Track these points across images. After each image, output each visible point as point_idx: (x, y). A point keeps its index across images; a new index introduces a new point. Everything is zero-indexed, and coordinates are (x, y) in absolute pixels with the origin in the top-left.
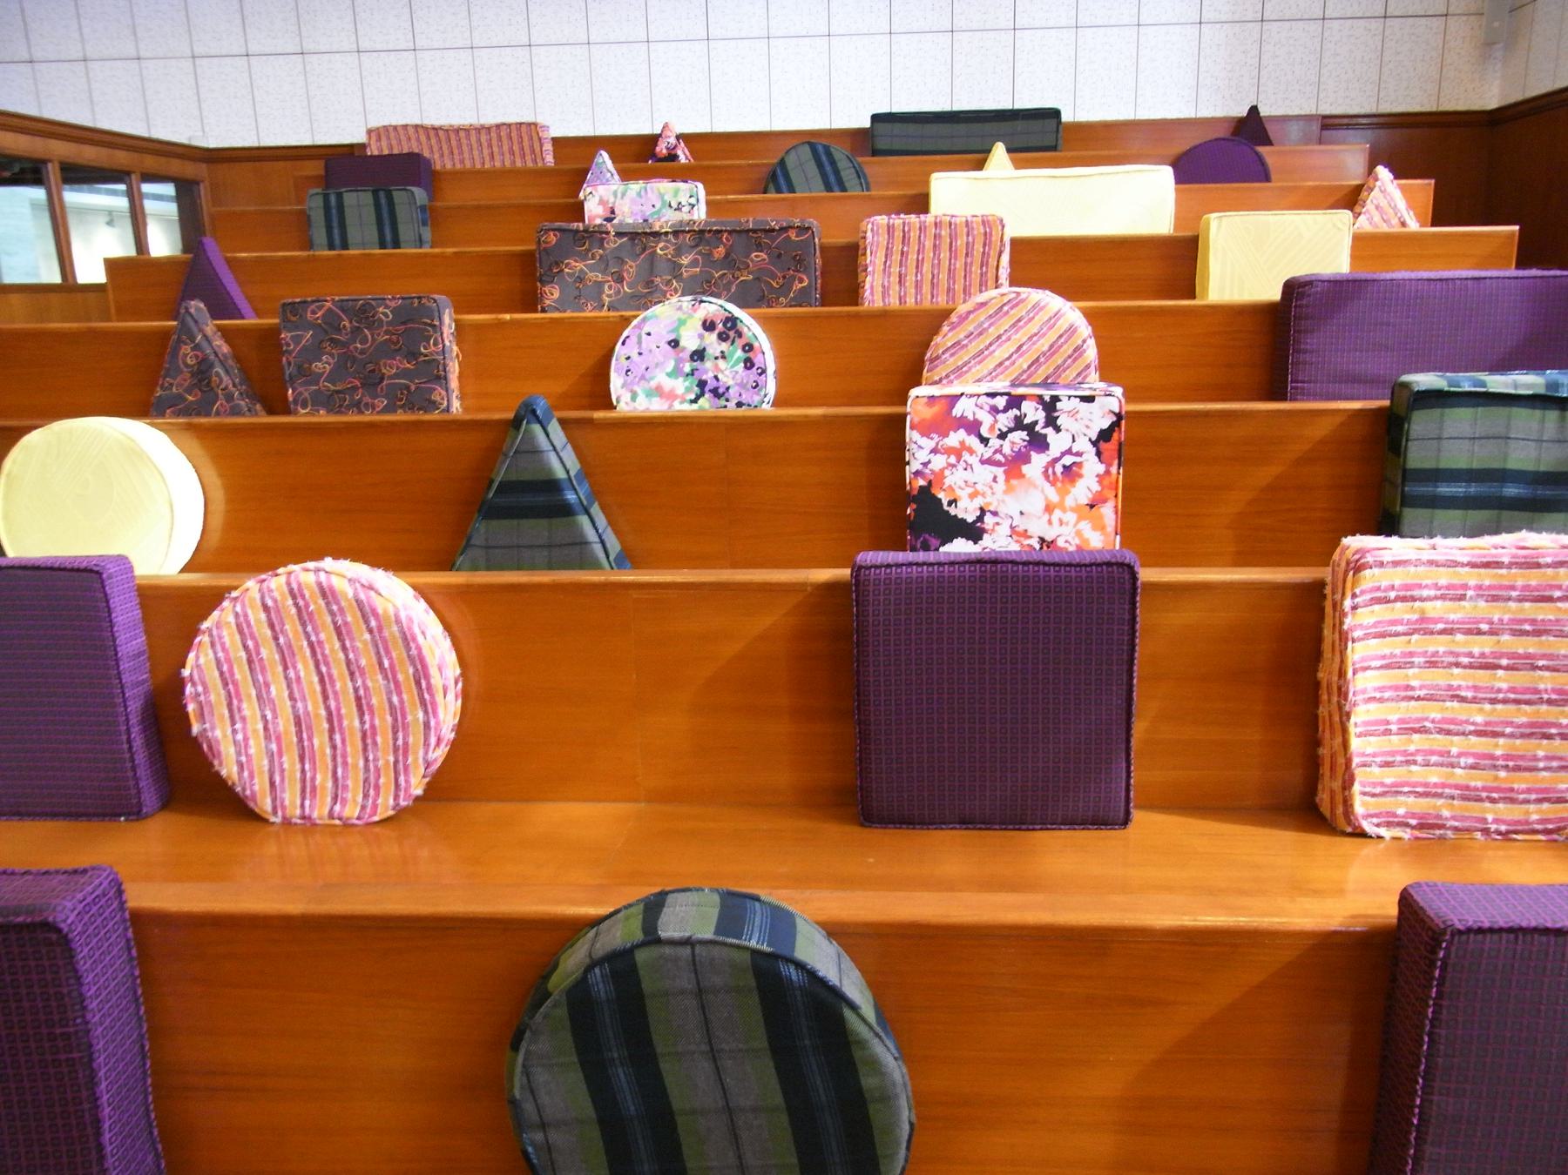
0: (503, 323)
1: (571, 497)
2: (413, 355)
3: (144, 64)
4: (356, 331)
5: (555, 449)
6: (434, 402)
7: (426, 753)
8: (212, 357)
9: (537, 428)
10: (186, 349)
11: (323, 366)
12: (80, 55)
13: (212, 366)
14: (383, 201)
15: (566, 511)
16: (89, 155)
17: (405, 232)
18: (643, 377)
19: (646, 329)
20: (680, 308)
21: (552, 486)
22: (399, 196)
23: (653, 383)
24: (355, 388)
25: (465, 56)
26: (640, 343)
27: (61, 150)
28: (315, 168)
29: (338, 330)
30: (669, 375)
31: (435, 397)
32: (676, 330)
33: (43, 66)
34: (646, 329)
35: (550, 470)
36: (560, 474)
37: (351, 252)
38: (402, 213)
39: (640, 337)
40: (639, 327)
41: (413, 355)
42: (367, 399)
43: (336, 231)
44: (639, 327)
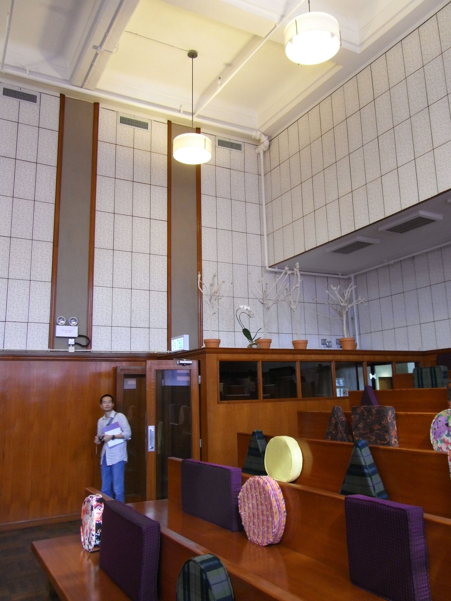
0: (407, 415)
1: (366, 471)
2: (380, 424)
3: (384, 332)
4: (368, 416)
5: (363, 456)
6: (386, 439)
7: (272, 530)
8: (338, 422)
9: (358, 449)
10: (333, 419)
11: (361, 426)
12: (448, 318)
13: (338, 424)
14: (433, 371)
15: (364, 475)
16: (378, 358)
17: (439, 381)
18: (439, 436)
19: (439, 419)
20: (448, 413)
21: (361, 467)
22: (437, 369)
23: (442, 438)
24: (368, 433)
25: (432, 324)
26: (438, 424)
27: (367, 358)
28: (434, 358)
29: (364, 415)
30: (446, 435)
31: (386, 437)
32: (447, 420)
33: (397, 329)
34: (439, 419)
35: (361, 462)
36: (363, 463)
37: (425, 389)
38: (438, 374)
39: (438, 422)
40: (437, 419)
41: (380, 424)
42: (371, 437)
43: (420, 381)
44: (437, 419)
